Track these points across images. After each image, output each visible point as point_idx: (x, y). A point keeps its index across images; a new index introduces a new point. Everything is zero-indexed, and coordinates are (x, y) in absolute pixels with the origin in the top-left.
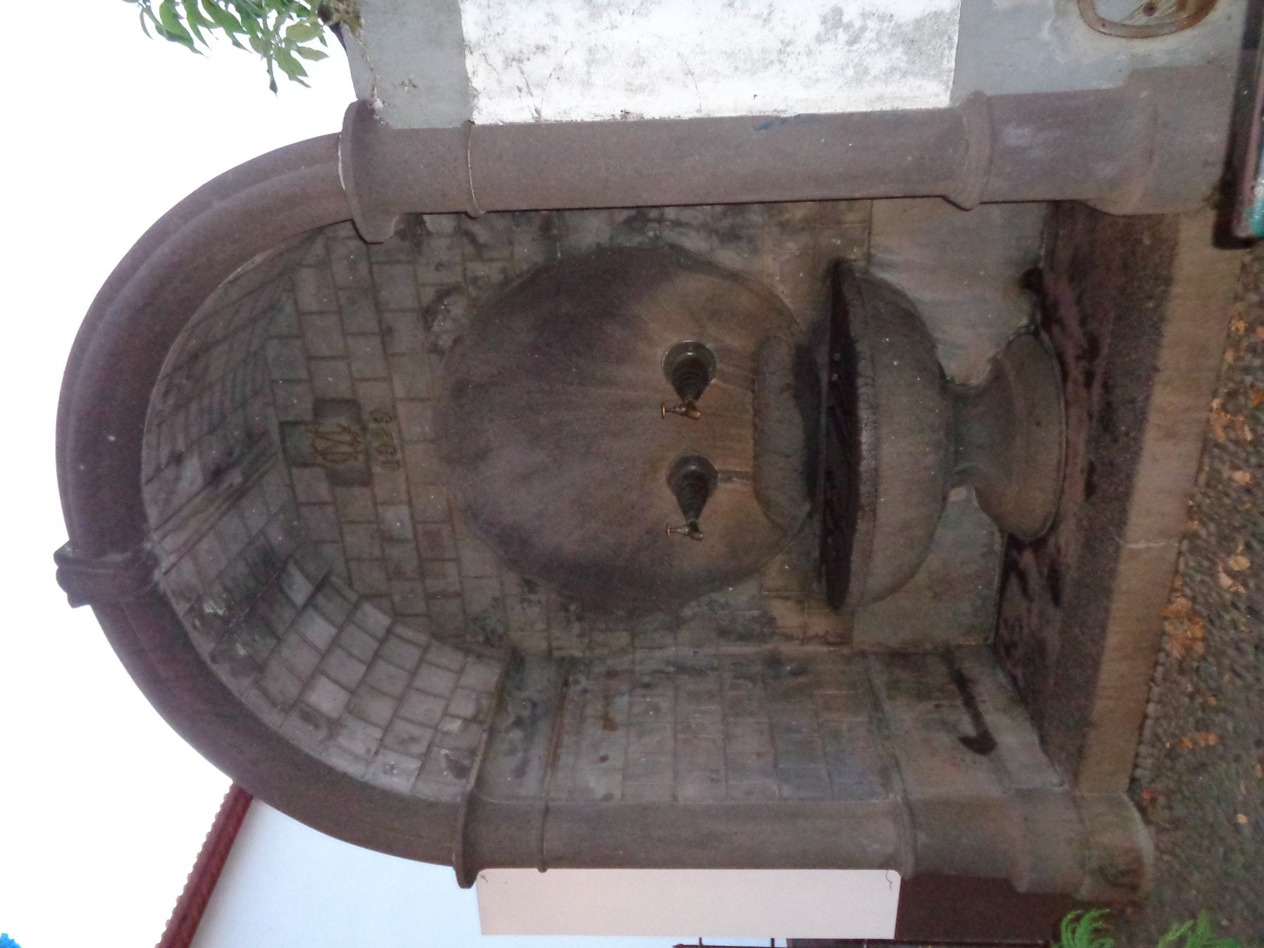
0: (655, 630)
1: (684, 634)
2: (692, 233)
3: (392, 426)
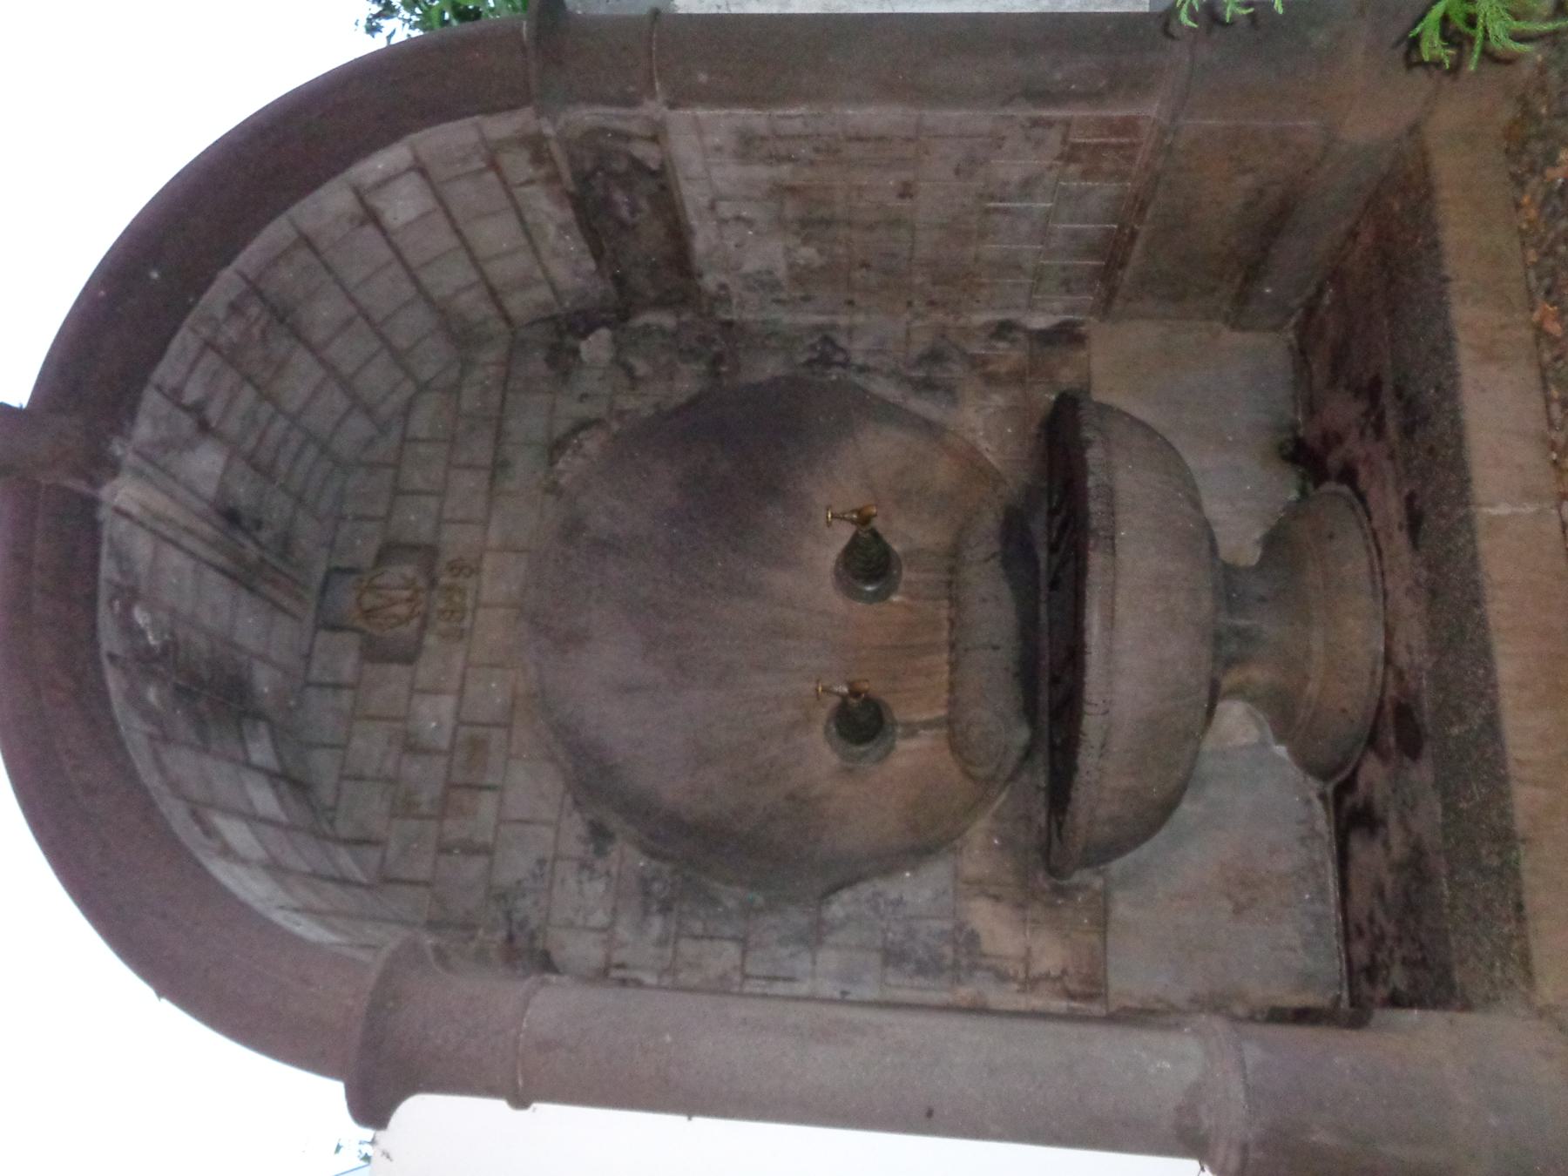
0: (782, 942)
1: (829, 959)
2: (880, 379)
3: (470, 583)
